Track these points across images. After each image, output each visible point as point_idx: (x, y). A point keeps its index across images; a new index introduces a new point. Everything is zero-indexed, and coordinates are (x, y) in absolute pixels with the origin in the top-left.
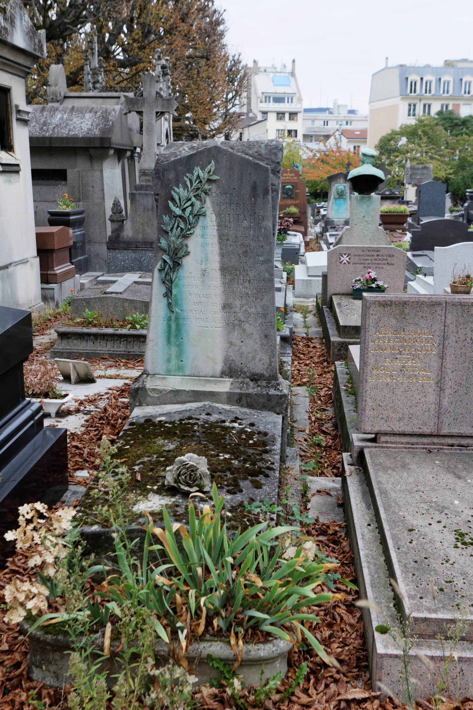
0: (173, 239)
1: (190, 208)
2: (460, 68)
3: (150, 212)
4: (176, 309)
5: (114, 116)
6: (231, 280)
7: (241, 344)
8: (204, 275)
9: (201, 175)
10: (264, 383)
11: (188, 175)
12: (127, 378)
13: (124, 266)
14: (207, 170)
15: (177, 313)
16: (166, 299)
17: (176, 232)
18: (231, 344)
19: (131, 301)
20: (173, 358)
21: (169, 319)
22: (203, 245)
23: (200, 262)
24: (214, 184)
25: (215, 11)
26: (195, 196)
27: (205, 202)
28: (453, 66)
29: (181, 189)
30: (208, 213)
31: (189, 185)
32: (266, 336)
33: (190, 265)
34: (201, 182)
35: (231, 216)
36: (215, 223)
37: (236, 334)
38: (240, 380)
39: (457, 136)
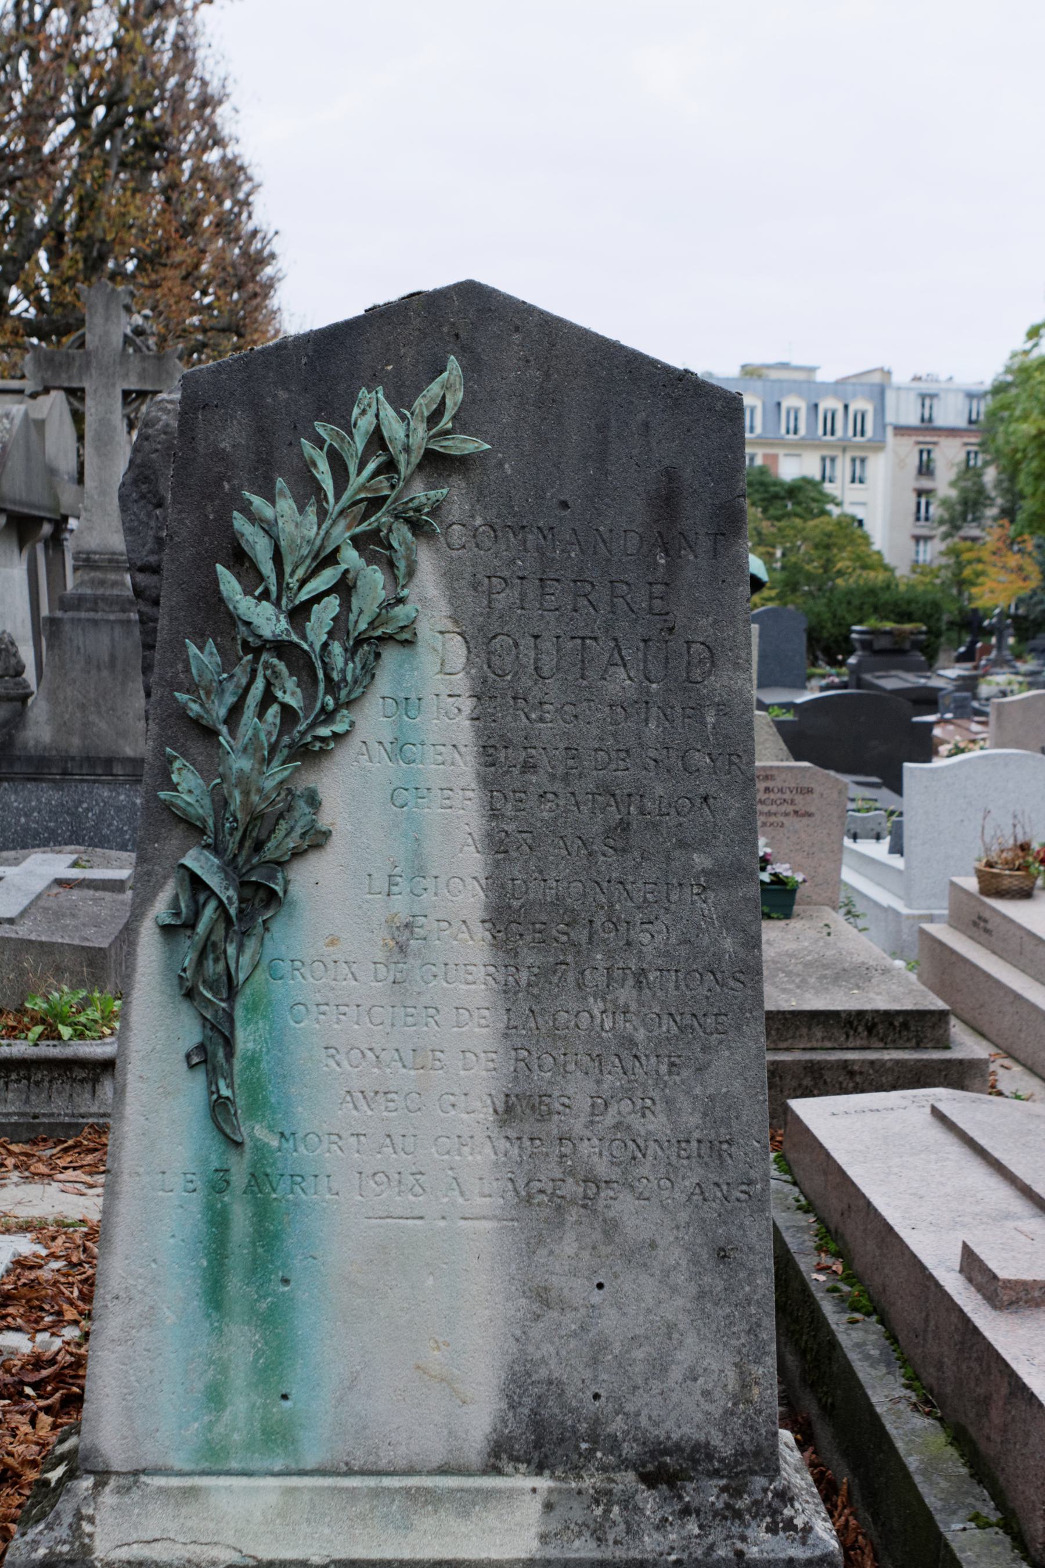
0: (241, 764)
1: (332, 605)
2: (774, 381)
3: (105, 673)
4: (256, 1131)
5: (8, 431)
6: (546, 972)
7: (597, 1297)
8: (402, 949)
9: (394, 428)
10: (711, 1493)
11: (321, 429)
12: (25, 1227)
13: (26, 829)
14: (424, 404)
15: (260, 1149)
16: (200, 1078)
17: (259, 726)
18: (543, 1297)
19: (45, 948)
20: (239, 1377)
21: (219, 1183)
22: (402, 796)
23: (381, 883)
24: (458, 482)
25: (255, 233)
26: (356, 541)
27: (411, 574)
28: (760, 376)
29: (286, 505)
30: (425, 630)
31: (328, 485)
32: (722, 1255)
33: (330, 898)
34: (389, 466)
35: (547, 645)
36: (461, 682)
37: (569, 1246)
38: (590, 1482)
39: (778, 519)
